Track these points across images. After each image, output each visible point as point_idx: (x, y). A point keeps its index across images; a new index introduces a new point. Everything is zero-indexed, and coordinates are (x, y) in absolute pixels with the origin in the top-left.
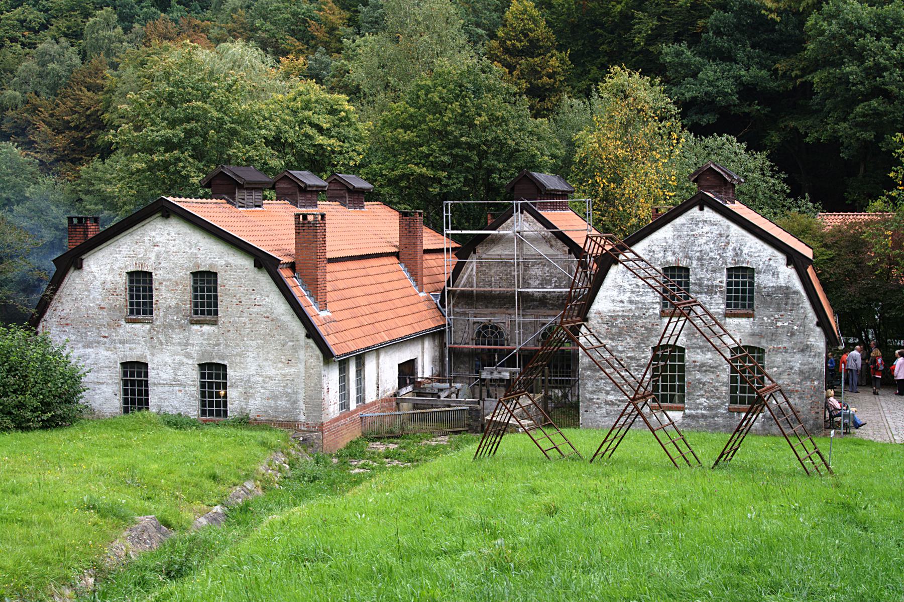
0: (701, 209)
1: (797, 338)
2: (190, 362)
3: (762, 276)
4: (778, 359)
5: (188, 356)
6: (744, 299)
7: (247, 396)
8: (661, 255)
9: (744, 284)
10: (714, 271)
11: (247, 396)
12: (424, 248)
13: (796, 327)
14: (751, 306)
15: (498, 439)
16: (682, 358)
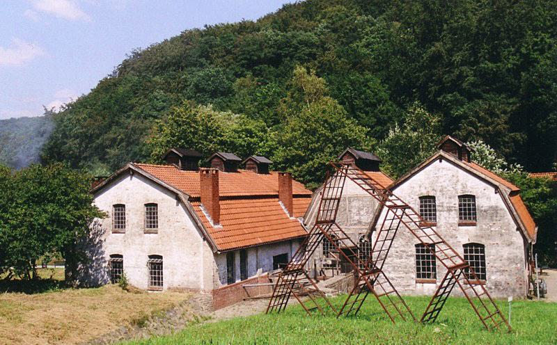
0: (441, 161)
1: (506, 237)
2: (144, 254)
3: (480, 200)
4: (493, 251)
5: (143, 251)
6: (430, 215)
7: (173, 274)
8: (418, 189)
9: (430, 206)
10: (450, 198)
11: (173, 274)
12: (293, 193)
13: (503, 231)
14: (475, 218)
15: (285, 301)
16: (483, 251)
